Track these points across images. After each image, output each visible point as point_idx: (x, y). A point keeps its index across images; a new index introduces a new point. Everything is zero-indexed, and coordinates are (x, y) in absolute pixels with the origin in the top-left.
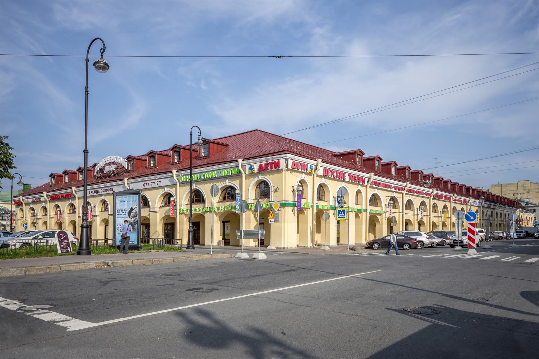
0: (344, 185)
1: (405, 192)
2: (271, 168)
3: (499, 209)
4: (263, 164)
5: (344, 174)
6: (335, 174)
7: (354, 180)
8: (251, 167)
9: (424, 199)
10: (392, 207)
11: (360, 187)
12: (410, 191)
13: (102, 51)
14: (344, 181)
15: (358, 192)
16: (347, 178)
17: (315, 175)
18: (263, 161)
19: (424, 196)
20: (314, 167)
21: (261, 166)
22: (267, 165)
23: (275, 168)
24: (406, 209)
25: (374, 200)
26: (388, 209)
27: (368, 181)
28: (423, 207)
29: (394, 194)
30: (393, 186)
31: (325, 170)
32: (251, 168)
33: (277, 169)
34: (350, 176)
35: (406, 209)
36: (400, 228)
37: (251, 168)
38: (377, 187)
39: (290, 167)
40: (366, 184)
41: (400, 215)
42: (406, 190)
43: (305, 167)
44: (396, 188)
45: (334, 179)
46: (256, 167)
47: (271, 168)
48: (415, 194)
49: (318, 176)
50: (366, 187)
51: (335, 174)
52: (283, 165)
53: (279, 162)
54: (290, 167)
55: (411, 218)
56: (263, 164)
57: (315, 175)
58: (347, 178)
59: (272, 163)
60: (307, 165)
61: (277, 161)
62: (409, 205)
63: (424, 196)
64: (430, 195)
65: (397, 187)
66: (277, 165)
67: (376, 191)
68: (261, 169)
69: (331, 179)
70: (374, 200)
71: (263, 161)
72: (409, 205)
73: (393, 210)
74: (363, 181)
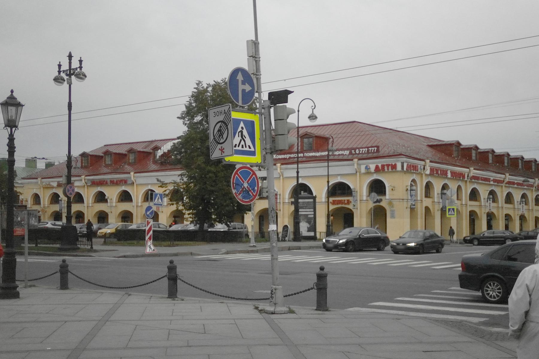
0: (446, 181)
1: (504, 185)
2: (388, 169)
3: (73, 164)
4: (380, 165)
5: (447, 171)
6: (439, 172)
7: (457, 176)
8: (367, 166)
9: (525, 191)
10: (491, 202)
11: (460, 183)
12: (474, 178)
13: (313, 108)
14: (447, 177)
15: (459, 187)
16: (449, 175)
17: (424, 175)
18: (379, 163)
19: (525, 187)
20: (422, 167)
21: (377, 167)
22: (383, 166)
23: (392, 169)
24: (506, 203)
25: (474, 195)
26: (487, 204)
27: (468, 176)
28: (524, 200)
29: (493, 188)
30: (492, 178)
31: (432, 170)
32: (367, 168)
33: (394, 170)
34: (453, 173)
35: (506, 203)
36: (500, 227)
37: (367, 168)
38: (476, 181)
39: (405, 169)
40: (466, 179)
41: (501, 209)
42: (505, 182)
43: (415, 168)
44: (495, 181)
45: (438, 177)
46: (372, 167)
47: (388, 169)
48: (516, 186)
49: (426, 175)
50: (466, 181)
51: (439, 172)
52: (399, 168)
53: (395, 165)
54: (405, 169)
55: (511, 212)
56: (380, 165)
57: (424, 175)
58: (449, 175)
59: (388, 166)
60: (418, 166)
61: (393, 164)
62: (509, 199)
63: (525, 187)
64: (532, 186)
65: (496, 180)
66: (394, 167)
67: (475, 186)
68: (377, 169)
69: (435, 177)
70: (474, 195)
71: (380, 162)
72: (509, 199)
73: (493, 205)
74: (464, 177)
